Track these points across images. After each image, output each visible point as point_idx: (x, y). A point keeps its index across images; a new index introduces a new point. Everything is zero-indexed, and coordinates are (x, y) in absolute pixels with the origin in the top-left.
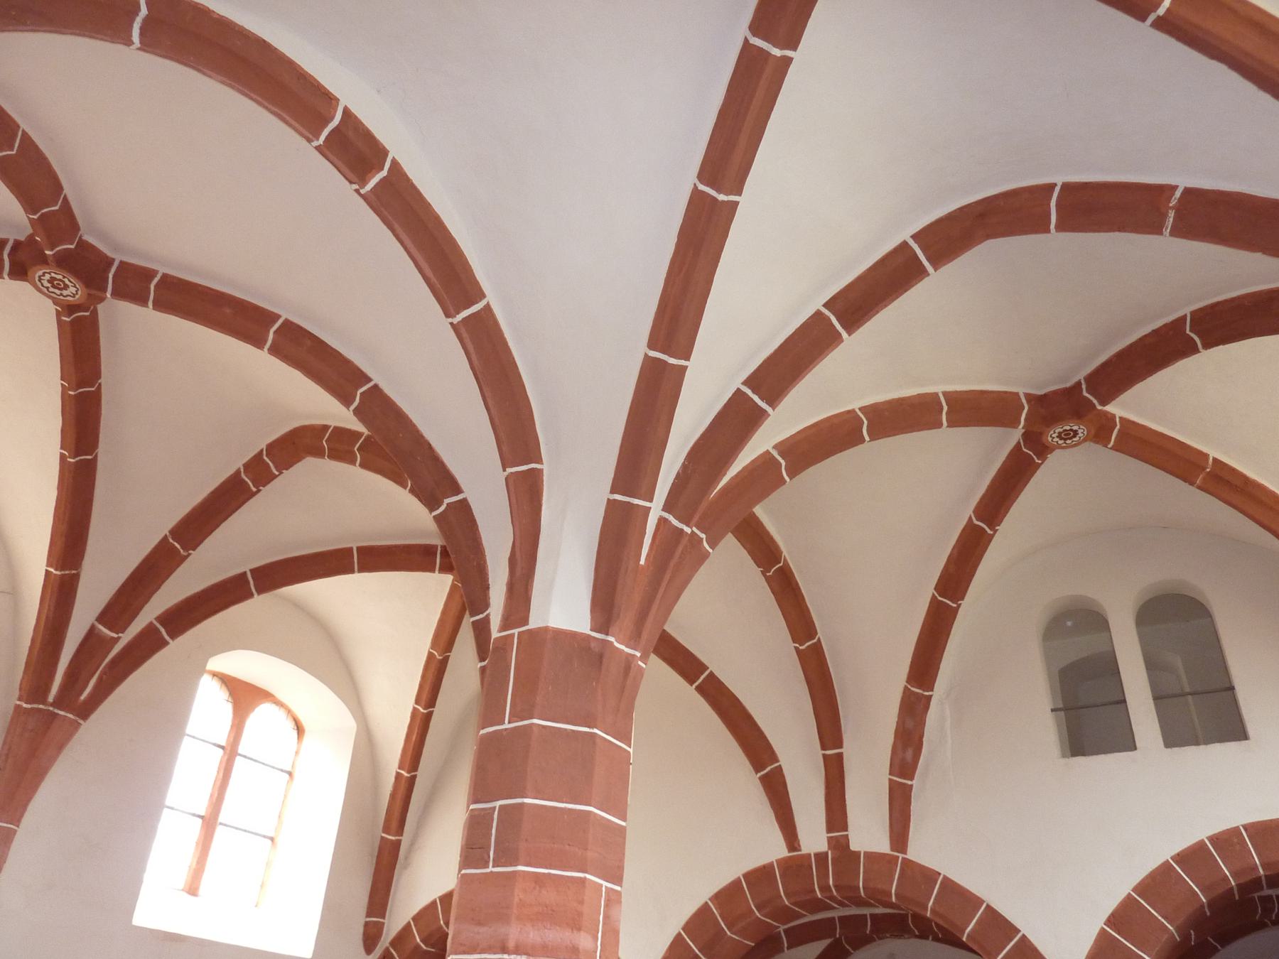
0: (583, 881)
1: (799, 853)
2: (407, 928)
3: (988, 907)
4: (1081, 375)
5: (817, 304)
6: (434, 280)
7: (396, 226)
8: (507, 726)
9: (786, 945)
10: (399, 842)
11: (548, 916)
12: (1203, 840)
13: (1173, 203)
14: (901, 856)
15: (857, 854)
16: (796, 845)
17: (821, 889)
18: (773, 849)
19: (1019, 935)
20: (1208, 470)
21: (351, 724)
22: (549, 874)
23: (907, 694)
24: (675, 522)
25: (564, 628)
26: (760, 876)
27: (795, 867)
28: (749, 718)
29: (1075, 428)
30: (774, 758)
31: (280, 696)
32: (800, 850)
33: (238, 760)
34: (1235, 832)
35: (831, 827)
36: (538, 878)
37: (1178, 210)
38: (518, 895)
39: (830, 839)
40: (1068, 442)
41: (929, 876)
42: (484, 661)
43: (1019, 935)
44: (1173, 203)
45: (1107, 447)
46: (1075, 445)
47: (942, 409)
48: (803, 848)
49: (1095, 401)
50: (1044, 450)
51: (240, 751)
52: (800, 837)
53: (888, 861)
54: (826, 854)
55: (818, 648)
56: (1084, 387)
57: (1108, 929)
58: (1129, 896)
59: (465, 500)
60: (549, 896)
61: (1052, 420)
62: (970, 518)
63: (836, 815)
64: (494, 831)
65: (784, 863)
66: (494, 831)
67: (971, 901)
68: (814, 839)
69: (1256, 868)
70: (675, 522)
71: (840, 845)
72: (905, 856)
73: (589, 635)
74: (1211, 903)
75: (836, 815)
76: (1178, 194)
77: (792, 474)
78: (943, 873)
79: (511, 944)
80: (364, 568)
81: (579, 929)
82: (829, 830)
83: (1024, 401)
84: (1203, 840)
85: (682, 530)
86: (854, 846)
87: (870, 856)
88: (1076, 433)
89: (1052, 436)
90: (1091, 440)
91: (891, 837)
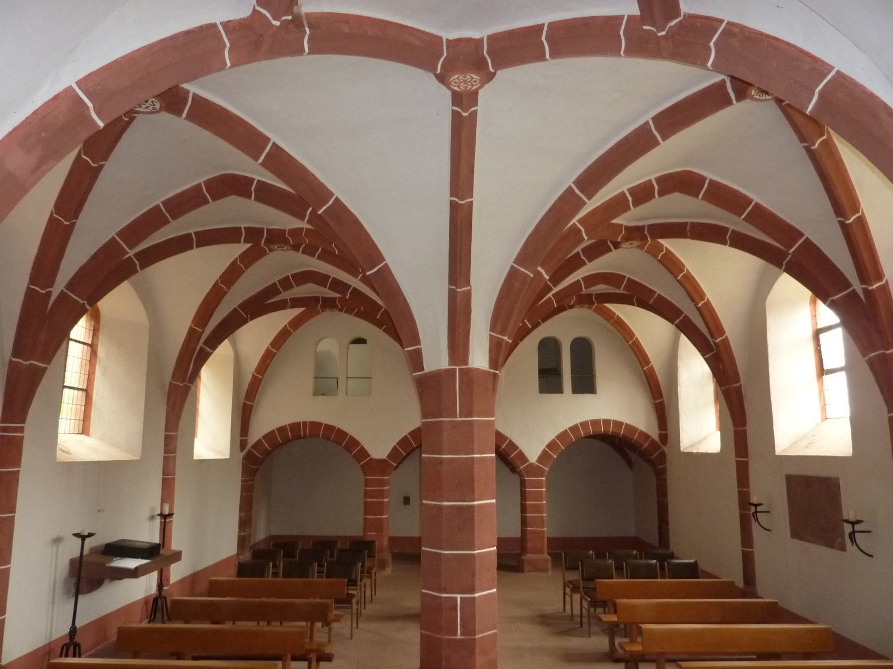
34: (587, 422)
58: (554, 439)
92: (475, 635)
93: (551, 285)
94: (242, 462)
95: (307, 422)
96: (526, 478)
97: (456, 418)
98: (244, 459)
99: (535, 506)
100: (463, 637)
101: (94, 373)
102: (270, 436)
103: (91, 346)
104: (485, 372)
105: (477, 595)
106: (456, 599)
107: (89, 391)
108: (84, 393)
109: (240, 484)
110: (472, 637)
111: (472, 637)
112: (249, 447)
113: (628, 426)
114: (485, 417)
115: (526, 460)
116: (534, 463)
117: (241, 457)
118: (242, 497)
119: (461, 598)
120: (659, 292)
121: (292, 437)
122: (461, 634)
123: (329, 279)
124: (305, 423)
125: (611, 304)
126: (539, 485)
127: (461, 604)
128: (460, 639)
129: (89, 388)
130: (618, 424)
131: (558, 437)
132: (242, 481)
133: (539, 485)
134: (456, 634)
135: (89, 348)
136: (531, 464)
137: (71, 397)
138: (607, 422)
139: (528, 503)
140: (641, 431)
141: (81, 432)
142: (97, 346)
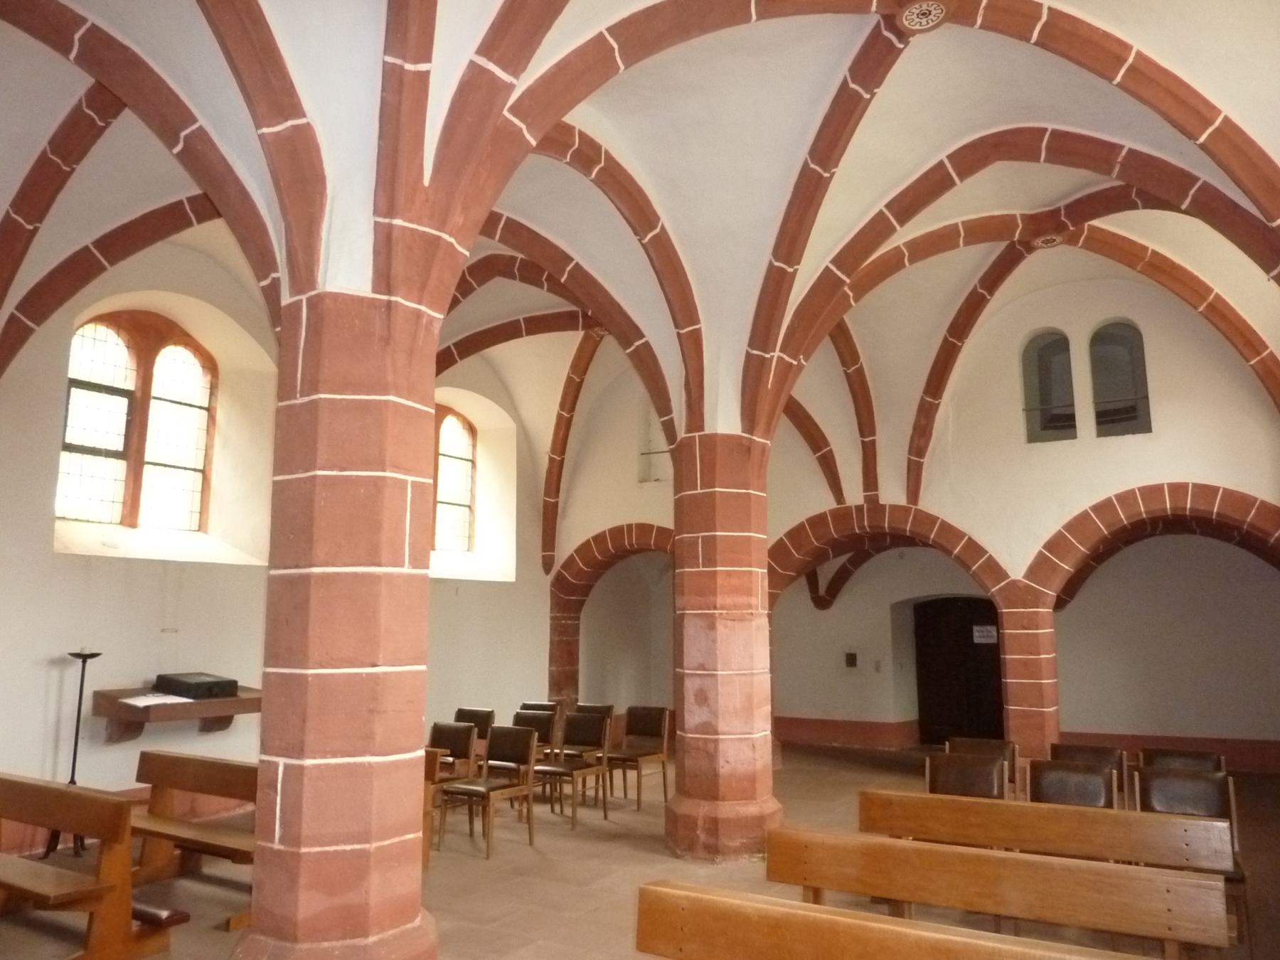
0: (750, 572)
1: (843, 506)
2: (571, 558)
3: (970, 539)
4: (1062, 204)
5: (881, 205)
6: (630, 218)
7: (611, 194)
8: (699, 491)
9: (831, 556)
10: (557, 502)
11: (736, 591)
12: (1111, 497)
13: (1120, 159)
14: (914, 507)
15: (883, 507)
16: (842, 500)
17: (859, 528)
18: (824, 502)
19: (988, 555)
20: (1146, 260)
21: (511, 425)
22: (734, 570)
23: (922, 402)
24: (787, 359)
25: (728, 433)
26: (817, 521)
27: (842, 515)
28: (809, 417)
29: (1054, 238)
30: (826, 443)
31: (457, 409)
32: (845, 504)
33: (441, 458)
34: (1132, 492)
35: (866, 489)
36: (729, 573)
37: (1122, 165)
38: (719, 581)
39: (866, 497)
40: (1049, 245)
41: (932, 519)
42: (673, 444)
43: (988, 555)
44: (1120, 159)
45: (1112, 84)
46: (1055, 246)
47: (960, 235)
48: (847, 502)
49: (1069, 224)
50: (1030, 249)
51: (441, 452)
52: (845, 495)
53: (906, 510)
54: (863, 505)
55: (860, 372)
56: (1063, 212)
57: (1045, 551)
58: (1060, 532)
59: (647, 342)
60: (735, 581)
61: (1037, 234)
62: (976, 286)
63: (870, 480)
64: (700, 549)
65: (834, 513)
66: (700, 549)
67: (959, 534)
68: (854, 495)
69: (1141, 514)
70: (787, 359)
71: (873, 501)
72: (917, 507)
73: (741, 436)
74: (1110, 533)
75: (870, 480)
76: (1124, 152)
77: (857, 300)
78: (941, 517)
79: (718, 605)
80: (530, 332)
81: (751, 595)
82: (865, 490)
83: (1019, 221)
84: (1111, 497)
85: (792, 363)
86: (882, 502)
87: (895, 508)
88: (1054, 240)
89: (1038, 242)
90: (1065, 243)
91: (908, 494)
92: (299, 847)
93: (820, 170)
94: (551, 590)
95: (632, 525)
96: (1004, 610)
97: (296, 398)
98: (553, 585)
99: (1026, 663)
100: (282, 847)
101: (212, 447)
102: (584, 549)
103: (208, 409)
104: (360, 300)
105: (308, 762)
106: (276, 765)
107: (207, 472)
108: (199, 476)
109: (548, 621)
110: (294, 850)
111: (294, 850)
112: (557, 567)
113: (1228, 494)
114: (354, 394)
115: (1004, 575)
116: (1020, 581)
117: (549, 583)
118: (552, 643)
119: (286, 767)
120: (1129, 144)
121: (615, 550)
122: (282, 841)
123: (516, 263)
124: (630, 526)
125: (1102, 219)
126: (1033, 622)
127: (283, 778)
128: (279, 850)
129: (207, 468)
130: (1206, 491)
131: (1070, 527)
132: (552, 618)
133: (1033, 622)
134: (272, 841)
135: (205, 413)
136: (1014, 582)
137: (448, 522)
138: (1178, 489)
139: (1007, 657)
140: (1263, 503)
141: (197, 529)
142: (215, 409)
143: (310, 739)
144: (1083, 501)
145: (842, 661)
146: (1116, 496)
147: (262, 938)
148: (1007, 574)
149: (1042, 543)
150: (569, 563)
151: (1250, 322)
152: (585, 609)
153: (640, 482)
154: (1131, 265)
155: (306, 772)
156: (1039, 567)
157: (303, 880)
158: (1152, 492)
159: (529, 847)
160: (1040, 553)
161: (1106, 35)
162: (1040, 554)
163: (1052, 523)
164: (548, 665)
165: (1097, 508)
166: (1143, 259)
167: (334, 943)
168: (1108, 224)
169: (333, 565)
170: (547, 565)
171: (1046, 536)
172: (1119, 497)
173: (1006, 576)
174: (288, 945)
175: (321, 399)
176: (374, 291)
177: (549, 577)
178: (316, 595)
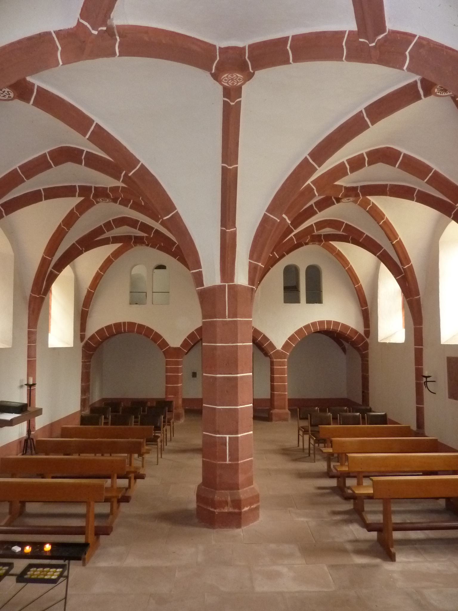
2: (93, 335)
3: (264, 335)
34: (316, 322)
94: (82, 349)
98: (83, 347)
102: (100, 332)
105: (239, 435)
106: (226, 438)
109: (81, 364)
112: (86, 339)
113: (343, 325)
119: (229, 438)
120: (367, 233)
122: (229, 461)
124: (124, 323)
126: (283, 364)
130: (337, 324)
133: (283, 364)
136: (278, 351)
140: (352, 328)
143: (240, 428)
144: (301, 325)
145: (191, 374)
146: (311, 323)
147: (223, 491)
148: (276, 348)
149: (288, 338)
150: (92, 338)
151: (357, 274)
152: (93, 357)
153: (130, 304)
154: (332, 253)
155: (239, 438)
156: (286, 346)
157: (240, 471)
158: (321, 323)
159: (161, 459)
160: (287, 341)
161: (381, 211)
162: (287, 341)
163: (291, 331)
164: (80, 383)
165: (305, 327)
166: (336, 252)
167: (246, 488)
168: (335, 244)
169: (243, 373)
170: (82, 338)
171: (289, 335)
172: (312, 324)
173: (275, 348)
174: (235, 491)
175: (238, 320)
176: (249, 284)
177: (82, 343)
178: (239, 383)
